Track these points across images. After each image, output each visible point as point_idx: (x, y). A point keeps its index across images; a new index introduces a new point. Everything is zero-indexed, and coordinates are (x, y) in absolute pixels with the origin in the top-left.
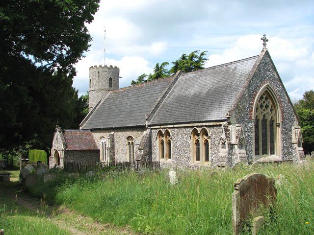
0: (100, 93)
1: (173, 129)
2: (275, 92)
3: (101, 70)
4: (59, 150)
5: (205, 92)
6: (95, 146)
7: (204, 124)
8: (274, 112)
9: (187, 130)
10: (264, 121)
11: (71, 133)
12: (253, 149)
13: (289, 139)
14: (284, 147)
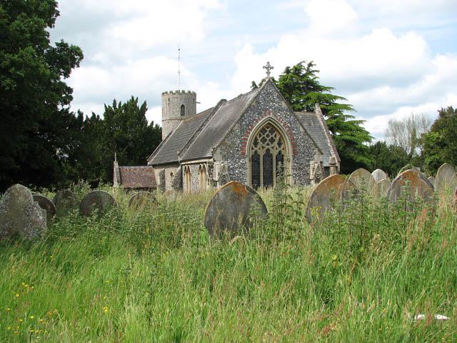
0: (171, 123)
3: (171, 96)
8: (282, 146)
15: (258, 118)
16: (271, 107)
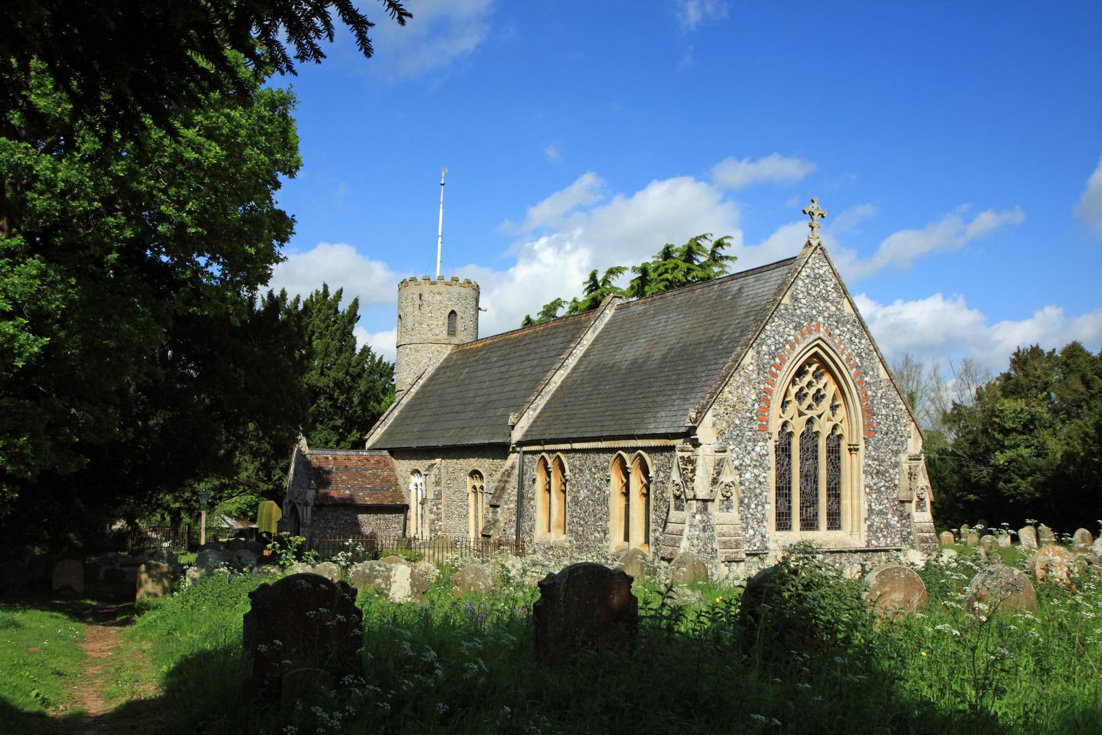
1: (571, 455)
2: (844, 358)
4: (299, 504)
5: (658, 355)
6: (398, 493)
7: (640, 443)
9: (603, 457)
10: (810, 437)
11: (335, 459)
12: (771, 510)
13: (888, 488)
14: (871, 510)
15: (796, 339)
16: (820, 313)
